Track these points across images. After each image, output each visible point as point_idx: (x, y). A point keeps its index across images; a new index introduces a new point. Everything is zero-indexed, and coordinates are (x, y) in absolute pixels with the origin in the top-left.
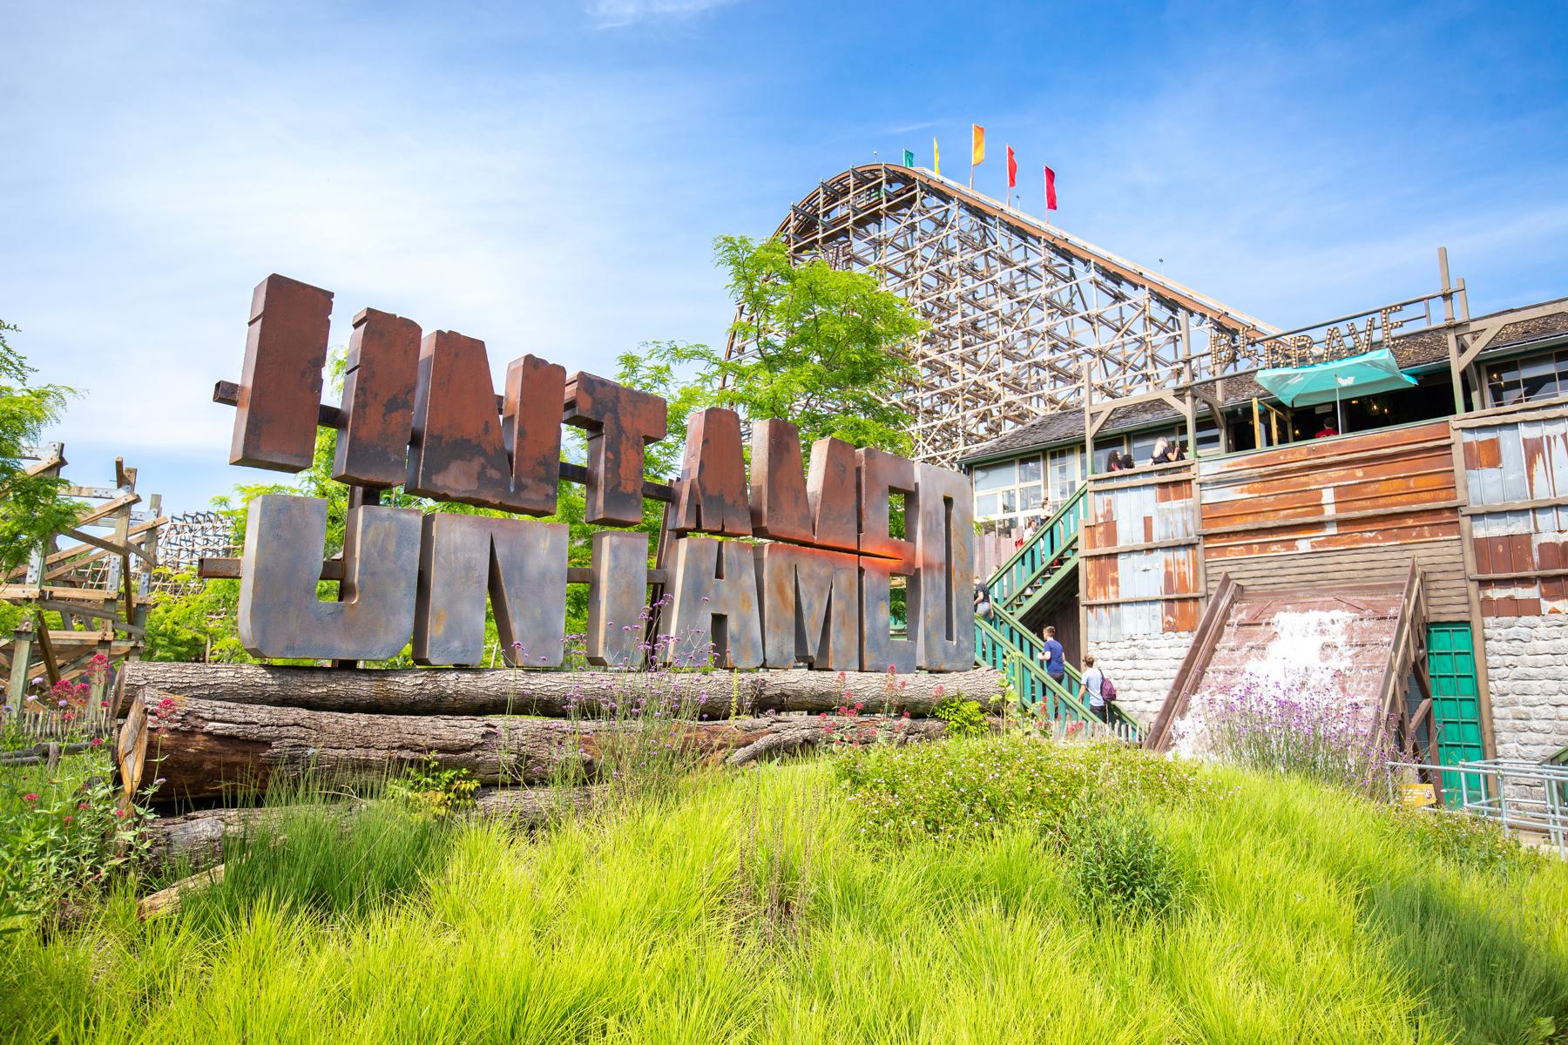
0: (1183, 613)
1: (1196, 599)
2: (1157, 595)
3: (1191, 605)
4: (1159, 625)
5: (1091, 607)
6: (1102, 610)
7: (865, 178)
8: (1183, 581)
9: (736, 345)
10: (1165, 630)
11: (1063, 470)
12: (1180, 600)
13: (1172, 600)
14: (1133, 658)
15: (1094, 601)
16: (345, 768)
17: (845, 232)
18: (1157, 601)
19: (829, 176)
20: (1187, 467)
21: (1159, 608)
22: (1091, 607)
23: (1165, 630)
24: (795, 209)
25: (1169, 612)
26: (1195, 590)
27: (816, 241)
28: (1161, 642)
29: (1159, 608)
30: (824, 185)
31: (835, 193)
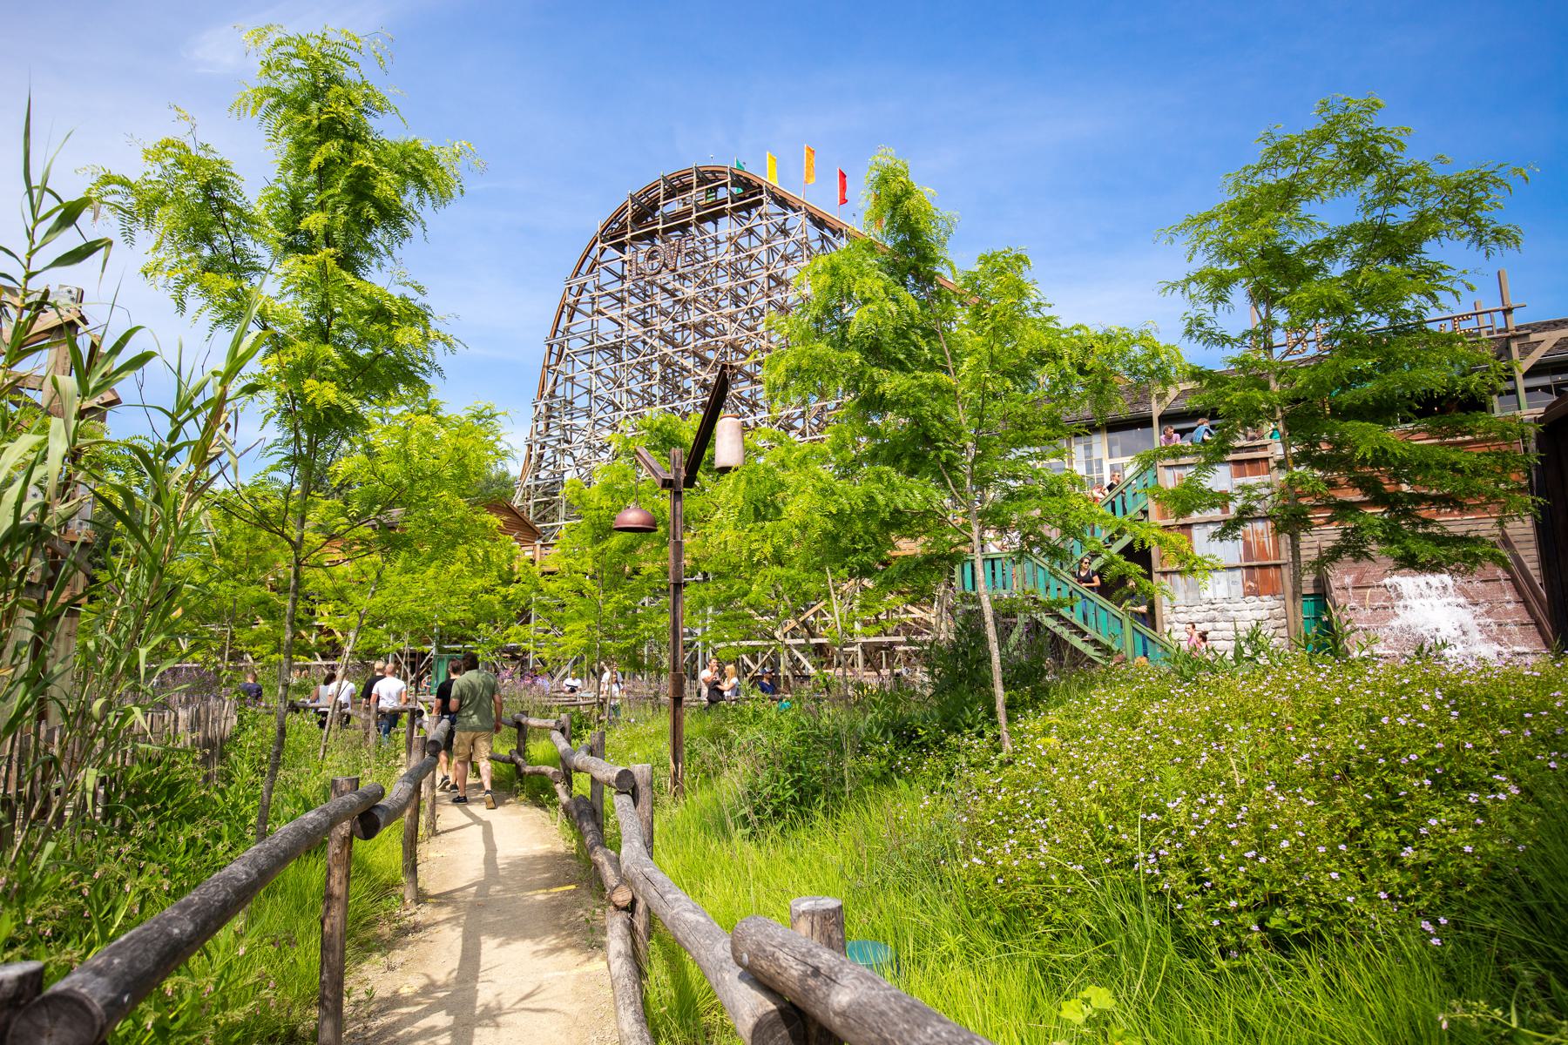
0: (1265, 580)
1: (1277, 566)
2: (1238, 563)
3: (1272, 572)
4: (1239, 589)
5: (1164, 574)
6: (1177, 577)
7: (708, 178)
8: (1262, 550)
9: (561, 328)
10: (1246, 595)
11: (1088, 448)
12: (1260, 567)
13: (1252, 567)
14: (1213, 620)
15: (1168, 568)
16: (1024, 703)
17: (688, 224)
18: (1238, 567)
19: (670, 169)
20: (1264, 447)
21: (1238, 575)
22: (1164, 574)
23: (1246, 595)
24: (632, 198)
25: (1250, 578)
26: (1278, 556)
27: (656, 231)
28: (1242, 605)
29: (1238, 575)
30: (664, 179)
31: (676, 188)
